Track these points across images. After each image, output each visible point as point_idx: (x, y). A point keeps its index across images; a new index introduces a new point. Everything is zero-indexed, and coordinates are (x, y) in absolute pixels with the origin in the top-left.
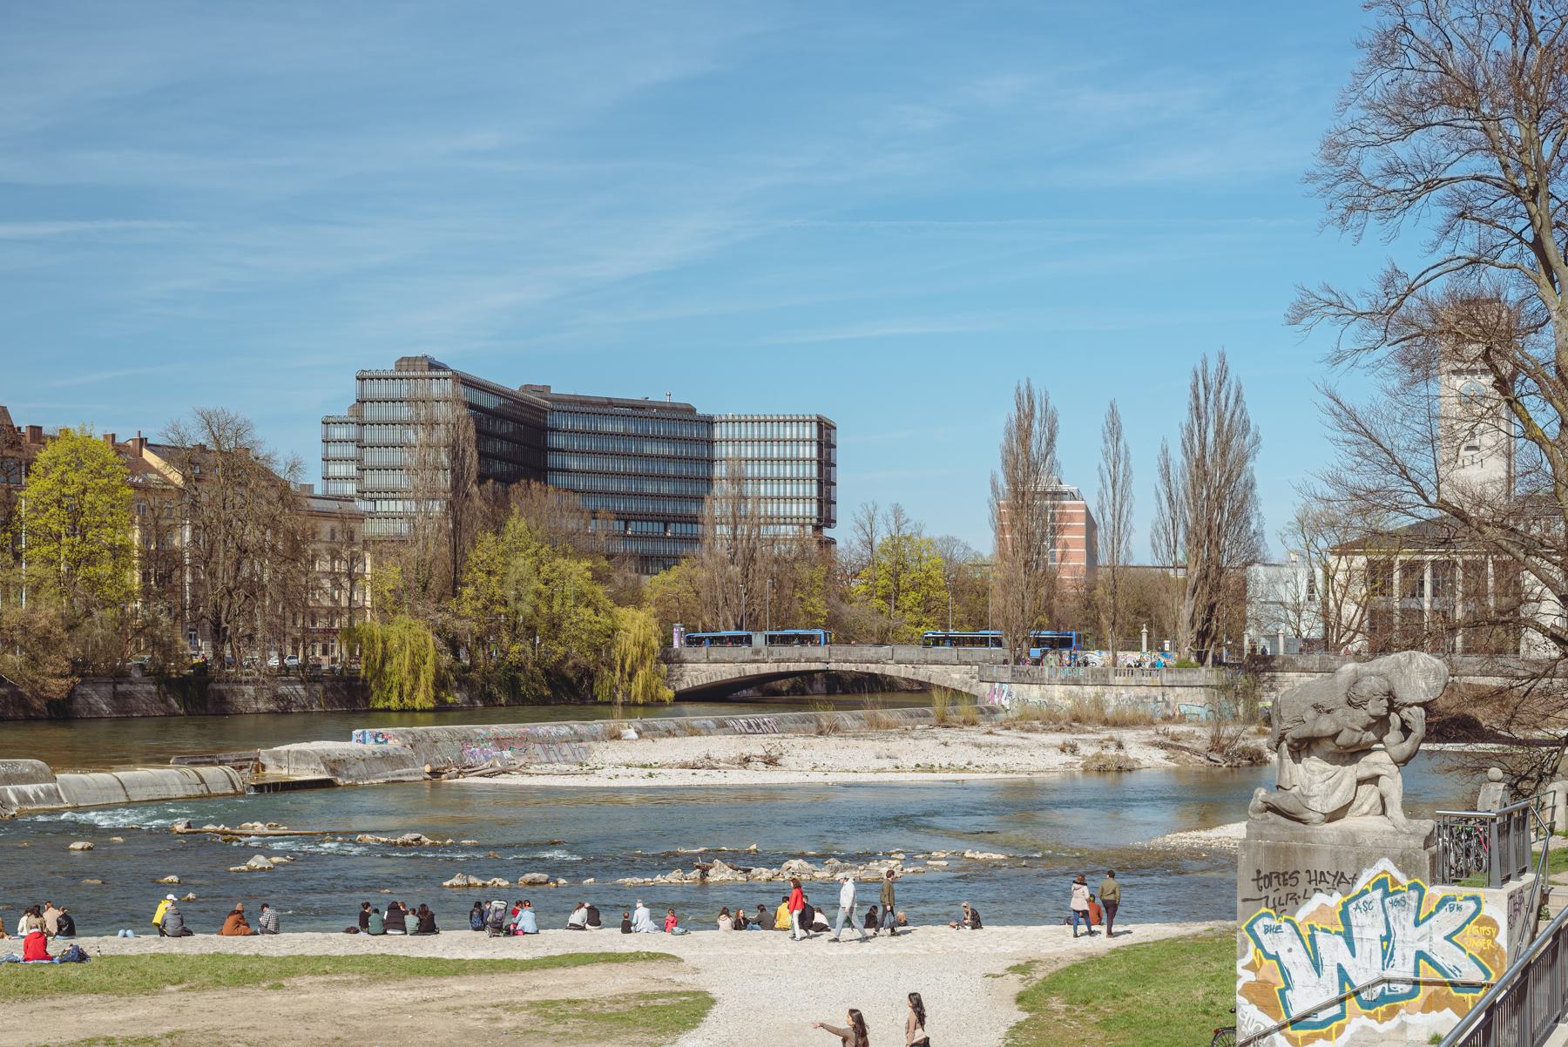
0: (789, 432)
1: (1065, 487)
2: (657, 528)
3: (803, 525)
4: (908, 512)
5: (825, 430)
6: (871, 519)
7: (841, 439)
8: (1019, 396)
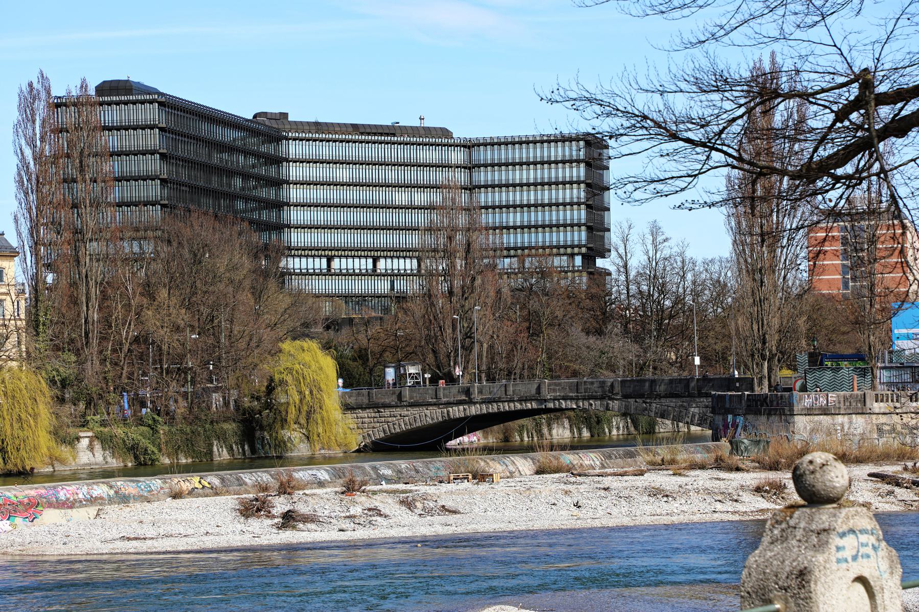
0: (557, 152)
3: (572, 255)
4: (667, 230)
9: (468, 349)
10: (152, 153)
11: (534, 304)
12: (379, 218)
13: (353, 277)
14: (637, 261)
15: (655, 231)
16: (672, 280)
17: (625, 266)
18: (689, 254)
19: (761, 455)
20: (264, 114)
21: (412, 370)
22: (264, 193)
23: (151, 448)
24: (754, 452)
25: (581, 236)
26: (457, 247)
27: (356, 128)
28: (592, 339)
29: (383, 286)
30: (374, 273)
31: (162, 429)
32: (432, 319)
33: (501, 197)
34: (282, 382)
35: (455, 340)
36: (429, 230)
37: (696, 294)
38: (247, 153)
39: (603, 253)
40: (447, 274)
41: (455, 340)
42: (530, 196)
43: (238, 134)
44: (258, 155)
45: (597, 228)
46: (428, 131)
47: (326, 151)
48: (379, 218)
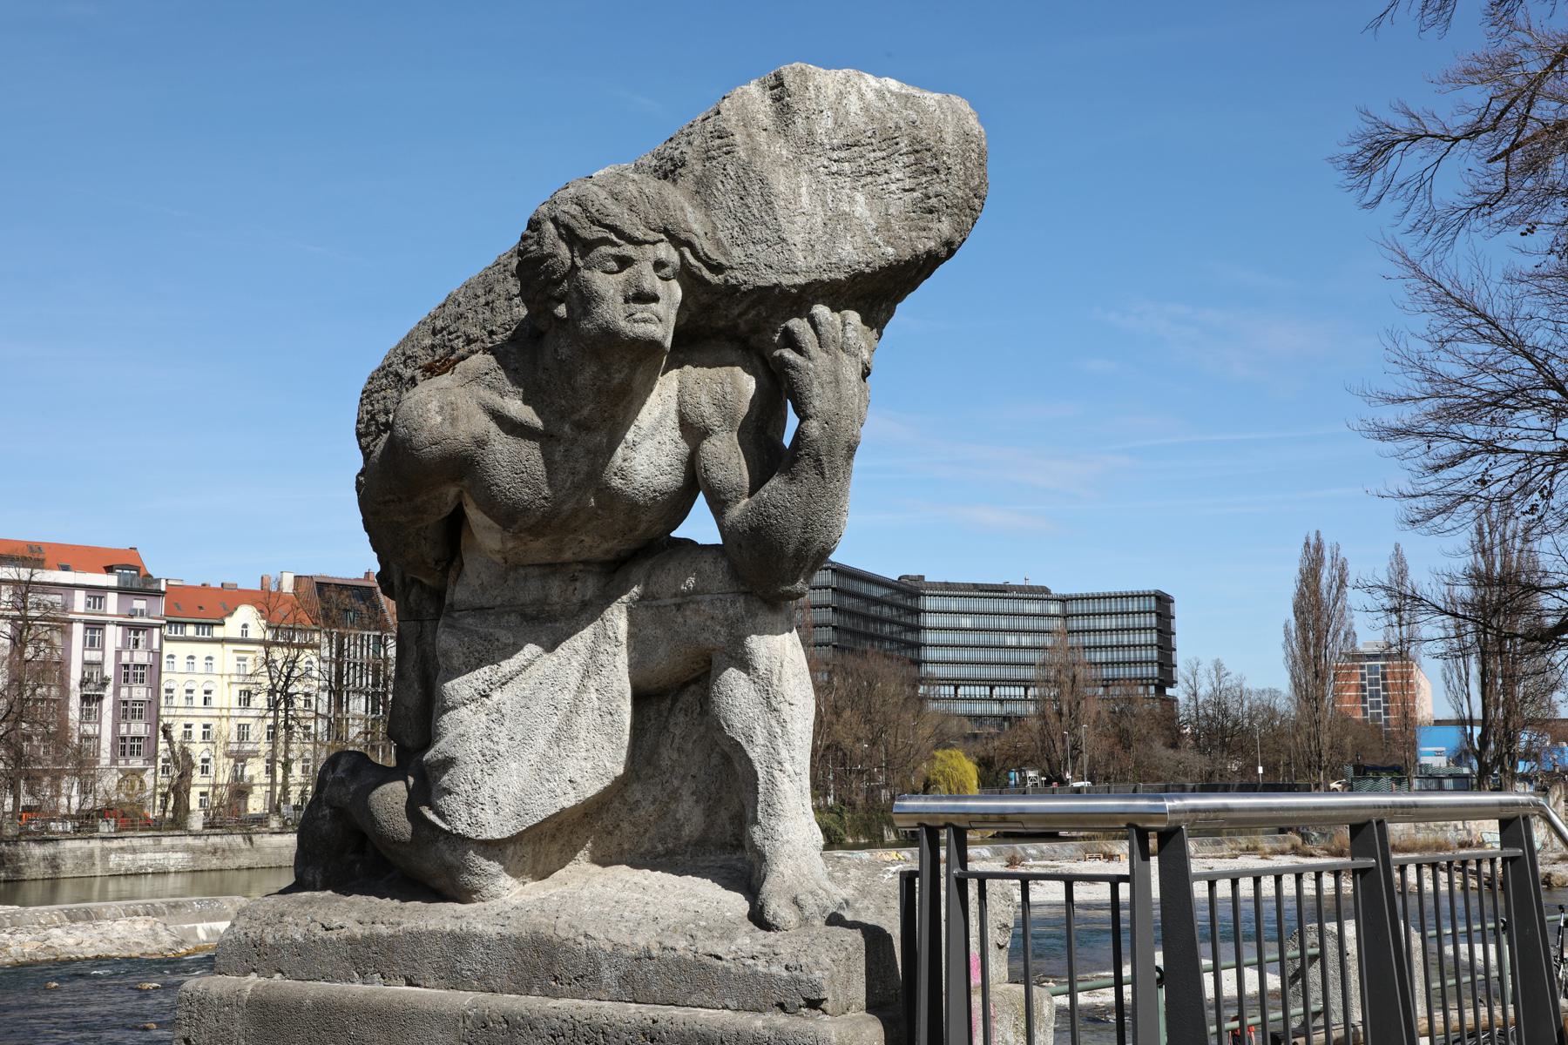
0: (1133, 605)
1: (1440, 662)
2: (983, 691)
3: (1147, 686)
4: (1228, 666)
5: (1163, 603)
6: (1194, 674)
7: (1178, 609)
8: (1307, 544)
9: (1075, 759)
10: (827, 607)
11: (1125, 723)
12: (995, 655)
13: (974, 701)
14: (1204, 690)
15: (1218, 666)
16: (1233, 707)
17: (1195, 695)
18: (1246, 685)
19: (1327, 845)
20: (907, 577)
21: (1031, 774)
22: (910, 637)
23: (840, 830)
24: (1323, 843)
25: (1154, 671)
26: (1065, 681)
27: (976, 587)
28: (1171, 751)
29: (996, 709)
30: (991, 699)
31: (847, 816)
32: (1045, 734)
33: (1089, 640)
34: (936, 782)
35: (1065, 751)
36: (1043, 665)
37: (1252, 718)
38: (891, 605)
39: (1172, 683)
40: (1056, 699)
41: (1065, 751)
42: (1113, 639)
43: (854, 601)
44: (899, 607)
45: (1166, 662)
46: (1032, 589)
47: (954, 604)
48: (995, 655)
